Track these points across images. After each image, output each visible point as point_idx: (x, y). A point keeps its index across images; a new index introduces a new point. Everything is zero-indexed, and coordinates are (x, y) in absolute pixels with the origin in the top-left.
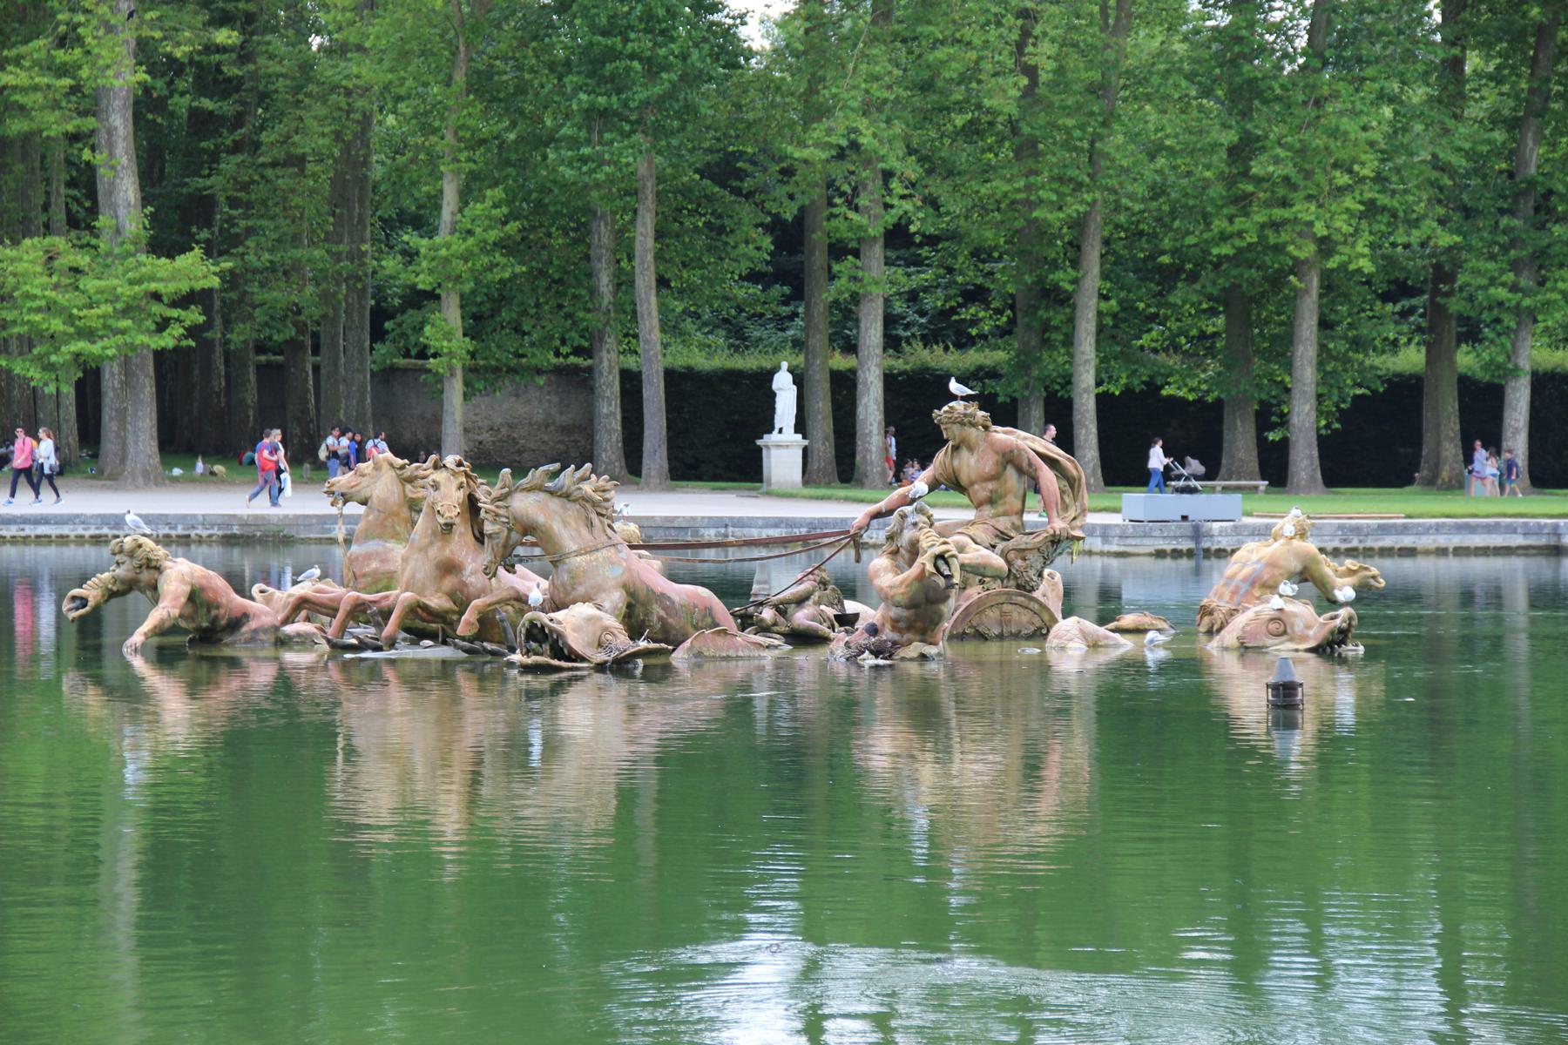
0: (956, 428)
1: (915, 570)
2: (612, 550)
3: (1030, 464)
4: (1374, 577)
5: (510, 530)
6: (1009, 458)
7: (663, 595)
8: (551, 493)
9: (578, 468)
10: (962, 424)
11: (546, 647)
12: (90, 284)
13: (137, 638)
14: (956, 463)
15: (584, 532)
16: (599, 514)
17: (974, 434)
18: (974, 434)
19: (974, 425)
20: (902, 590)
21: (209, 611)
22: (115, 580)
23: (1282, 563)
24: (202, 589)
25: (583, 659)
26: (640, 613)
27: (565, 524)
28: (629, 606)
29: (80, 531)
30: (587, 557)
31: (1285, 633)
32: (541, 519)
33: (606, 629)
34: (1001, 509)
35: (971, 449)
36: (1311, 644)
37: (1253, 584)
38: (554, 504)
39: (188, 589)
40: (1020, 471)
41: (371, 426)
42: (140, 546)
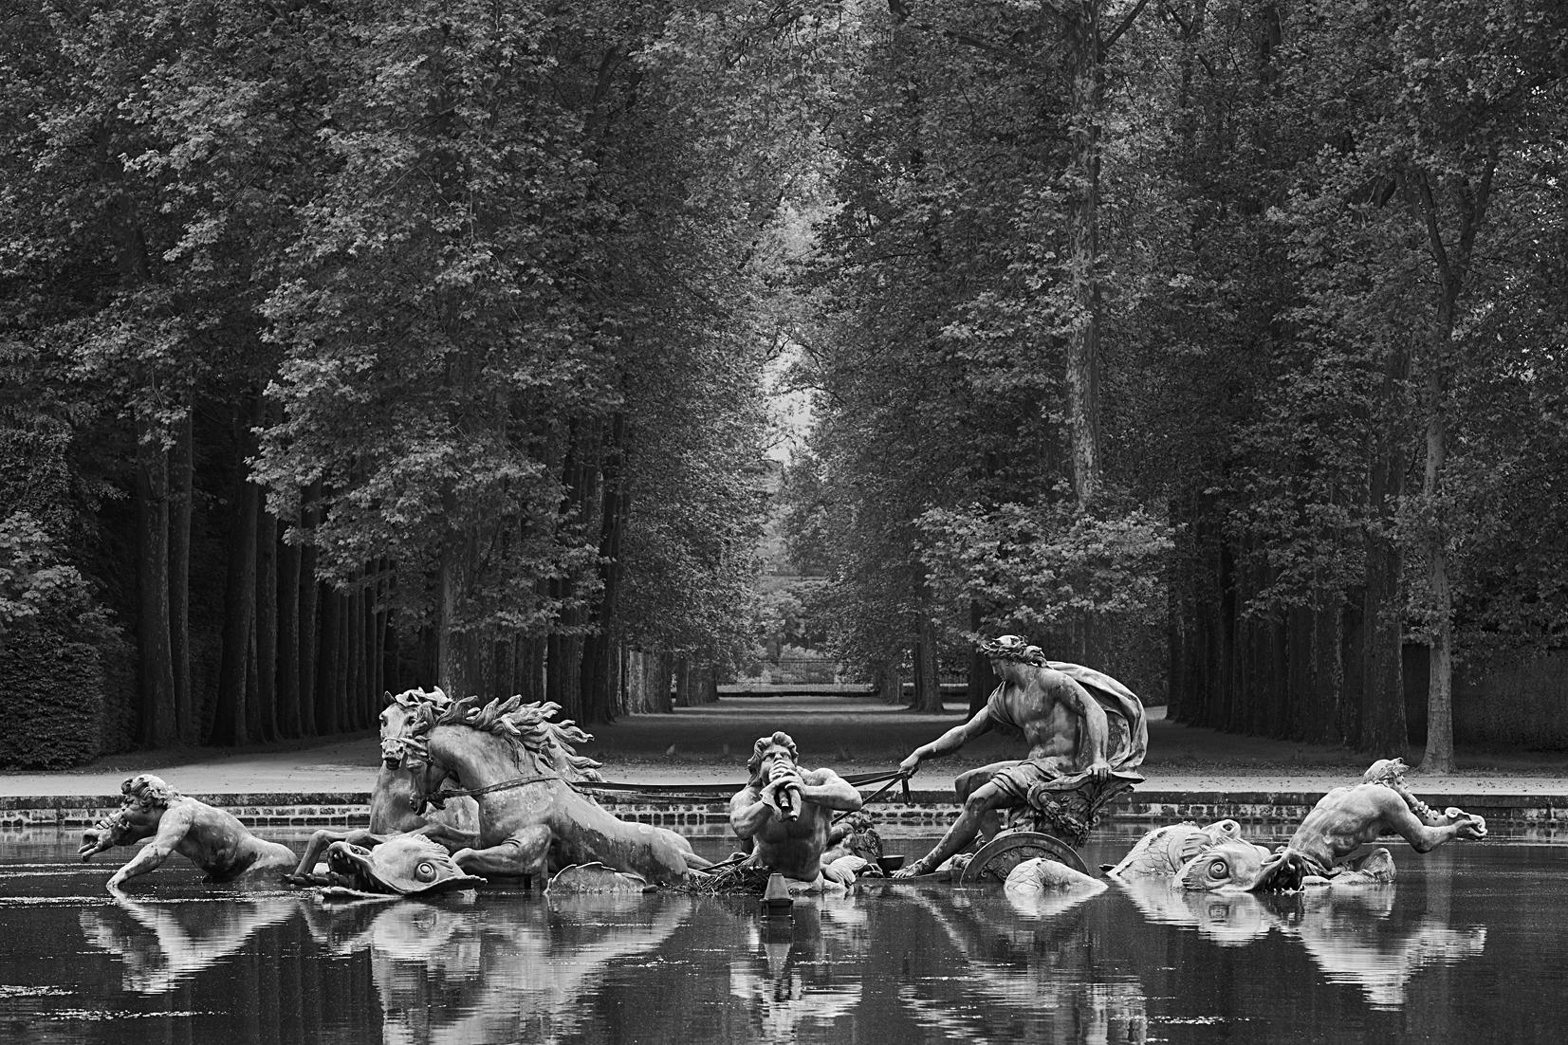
0: (1003, 664)
1: (759, 805)
2: (540, 785)
3: (1078, 701)
4: (1474, 826)
5: (430, 764)
6: (1056, 695)
7: (592, 831)
8: (474, 727)
9: (501, 702)
10: (1009, 659)
11: (352, 877)
12: (1039, 548)
13: (120, 875)
14: (1009, 700)
15: (509, 765)
16: (528, 749)
17: (1023, 669)
18: (1023, 669)
19: (1025, 660)
20: (746, 823)
21: (215, 852)
22: (125, 819)
23: (1356, 809)
24: (205, 828)
25: (390, 891)
26: (566, 847)
27: (486, 758)
28: (554, 842)
29: (892, 809)
30: (507, 792)
31: (1226, 875)
32: (458, 753)
33: (423, 861)
34: (1049, 749)
35: (1023, 687)
36: (1251, 886)
37: (1324, 831)
38: (477, 738)
39: (187, 827)
40: (1068, 707)
41: (1402, 706)
42: (146, 785)
